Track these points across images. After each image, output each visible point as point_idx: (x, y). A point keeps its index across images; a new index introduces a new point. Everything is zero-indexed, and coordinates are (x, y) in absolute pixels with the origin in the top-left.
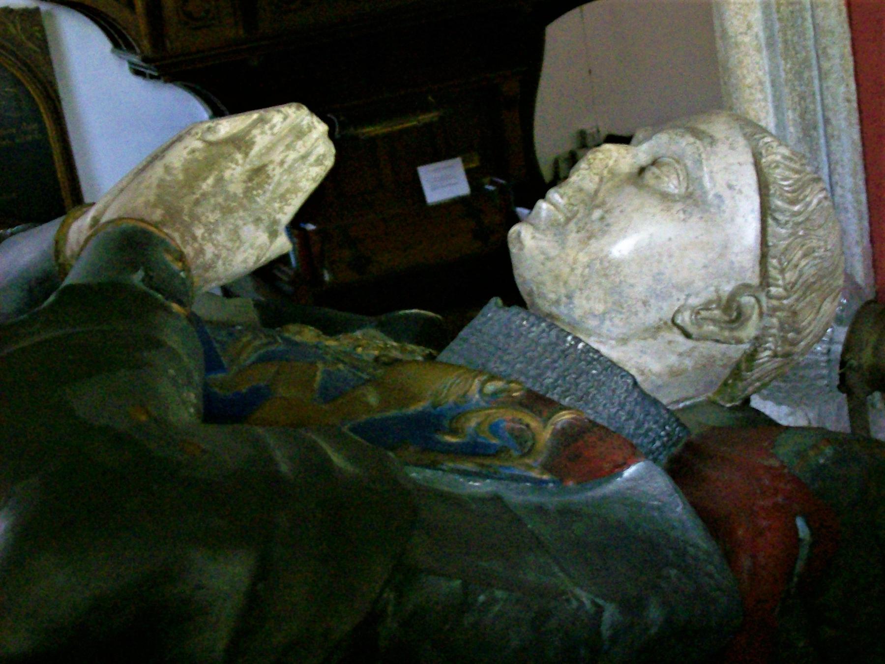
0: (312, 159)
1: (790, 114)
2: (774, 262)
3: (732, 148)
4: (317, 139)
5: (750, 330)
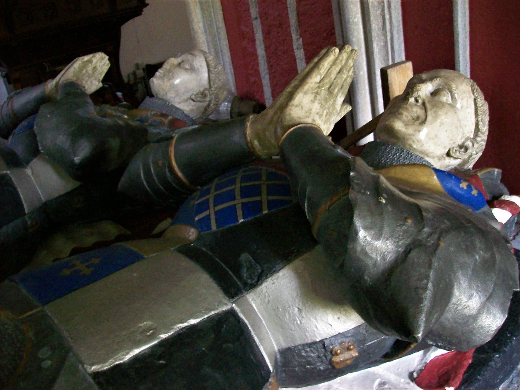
5: (208, 99)
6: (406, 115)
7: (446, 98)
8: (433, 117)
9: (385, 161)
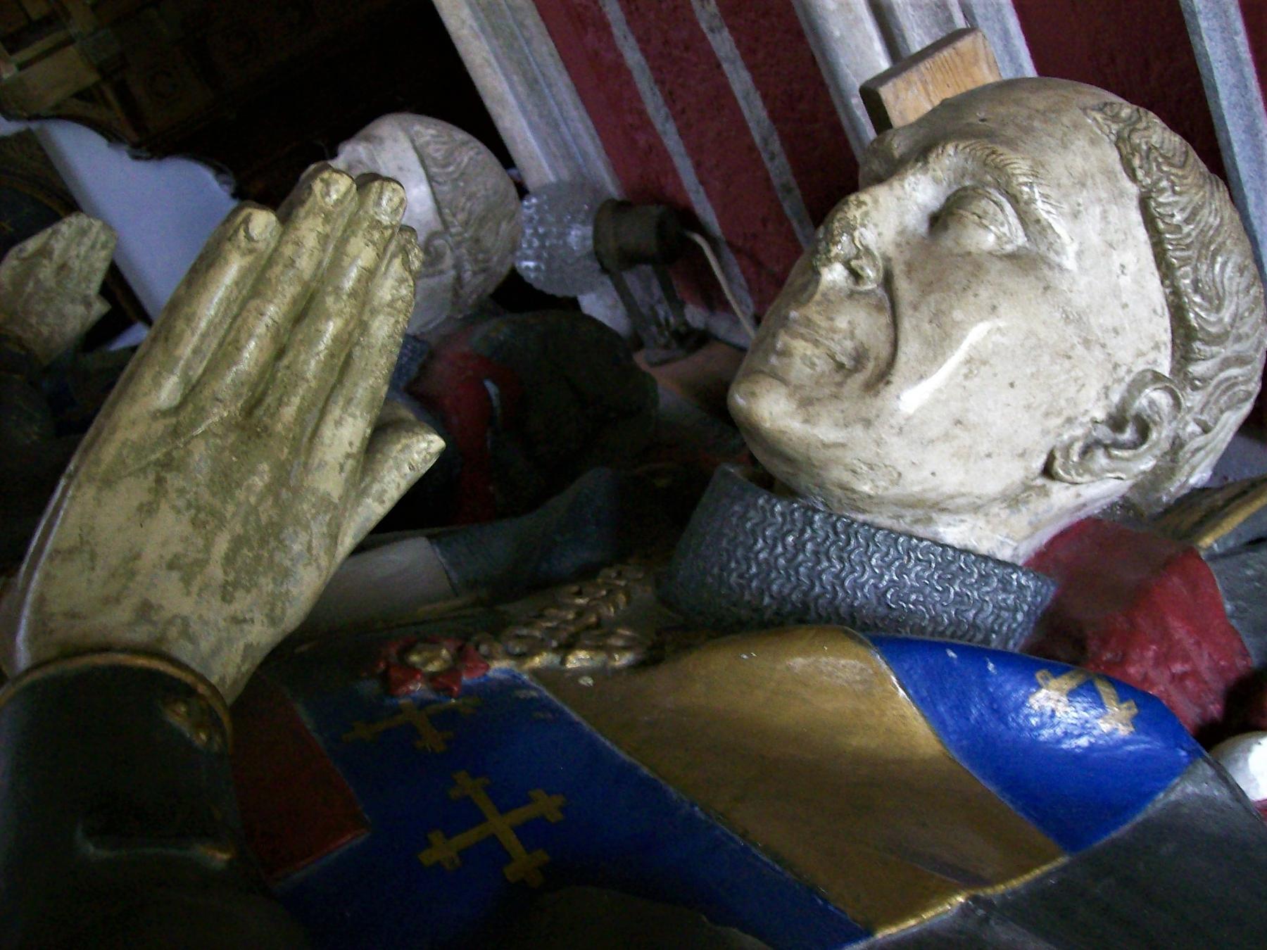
0: (99, 246)
1: (515, 78)
2: (447, 211)
3: (395, 140)
4: (98, 233)
5: (448, 261)
6: (804, 357)
7: (993, 231)
8: (928, 342)
9: (741, 576)
